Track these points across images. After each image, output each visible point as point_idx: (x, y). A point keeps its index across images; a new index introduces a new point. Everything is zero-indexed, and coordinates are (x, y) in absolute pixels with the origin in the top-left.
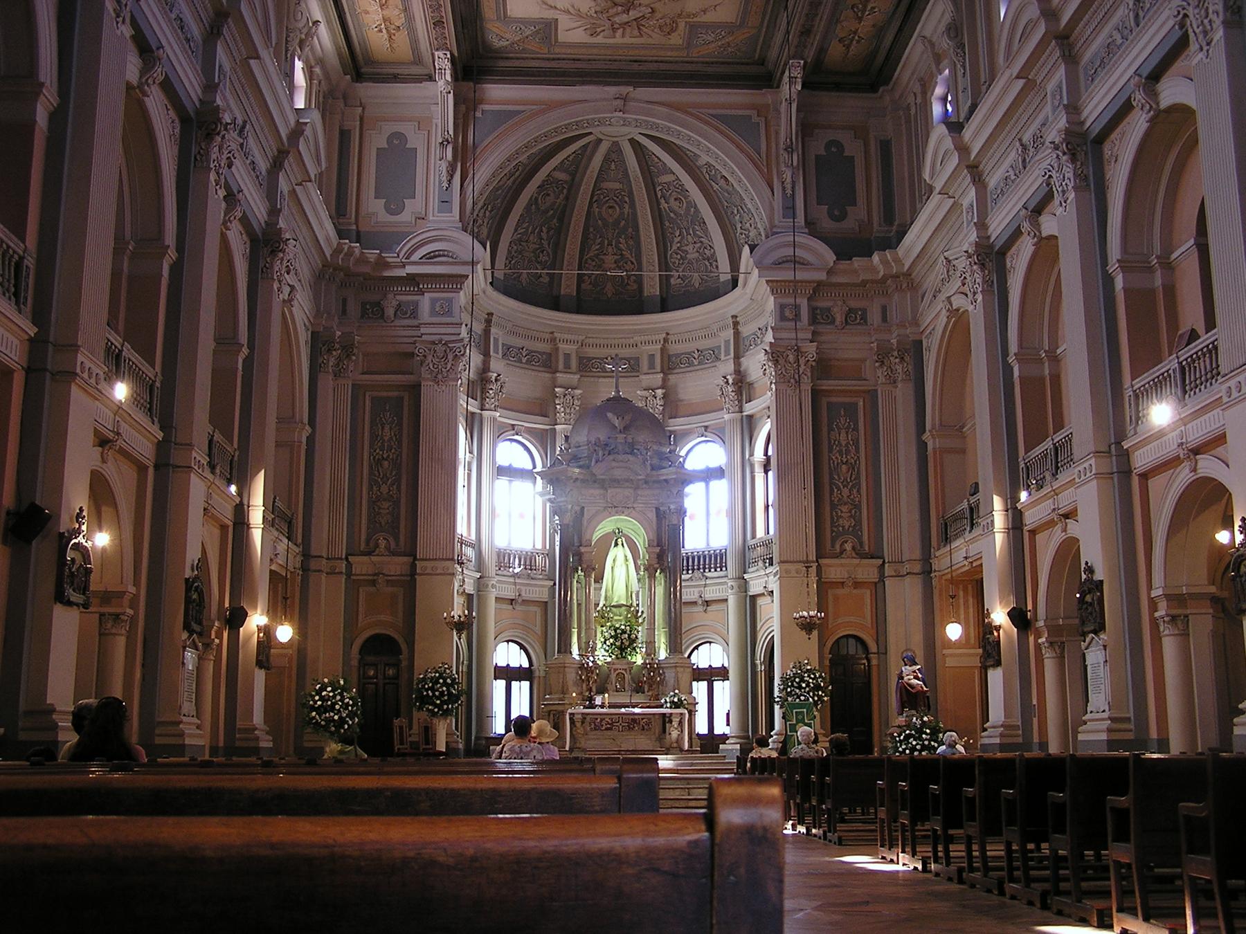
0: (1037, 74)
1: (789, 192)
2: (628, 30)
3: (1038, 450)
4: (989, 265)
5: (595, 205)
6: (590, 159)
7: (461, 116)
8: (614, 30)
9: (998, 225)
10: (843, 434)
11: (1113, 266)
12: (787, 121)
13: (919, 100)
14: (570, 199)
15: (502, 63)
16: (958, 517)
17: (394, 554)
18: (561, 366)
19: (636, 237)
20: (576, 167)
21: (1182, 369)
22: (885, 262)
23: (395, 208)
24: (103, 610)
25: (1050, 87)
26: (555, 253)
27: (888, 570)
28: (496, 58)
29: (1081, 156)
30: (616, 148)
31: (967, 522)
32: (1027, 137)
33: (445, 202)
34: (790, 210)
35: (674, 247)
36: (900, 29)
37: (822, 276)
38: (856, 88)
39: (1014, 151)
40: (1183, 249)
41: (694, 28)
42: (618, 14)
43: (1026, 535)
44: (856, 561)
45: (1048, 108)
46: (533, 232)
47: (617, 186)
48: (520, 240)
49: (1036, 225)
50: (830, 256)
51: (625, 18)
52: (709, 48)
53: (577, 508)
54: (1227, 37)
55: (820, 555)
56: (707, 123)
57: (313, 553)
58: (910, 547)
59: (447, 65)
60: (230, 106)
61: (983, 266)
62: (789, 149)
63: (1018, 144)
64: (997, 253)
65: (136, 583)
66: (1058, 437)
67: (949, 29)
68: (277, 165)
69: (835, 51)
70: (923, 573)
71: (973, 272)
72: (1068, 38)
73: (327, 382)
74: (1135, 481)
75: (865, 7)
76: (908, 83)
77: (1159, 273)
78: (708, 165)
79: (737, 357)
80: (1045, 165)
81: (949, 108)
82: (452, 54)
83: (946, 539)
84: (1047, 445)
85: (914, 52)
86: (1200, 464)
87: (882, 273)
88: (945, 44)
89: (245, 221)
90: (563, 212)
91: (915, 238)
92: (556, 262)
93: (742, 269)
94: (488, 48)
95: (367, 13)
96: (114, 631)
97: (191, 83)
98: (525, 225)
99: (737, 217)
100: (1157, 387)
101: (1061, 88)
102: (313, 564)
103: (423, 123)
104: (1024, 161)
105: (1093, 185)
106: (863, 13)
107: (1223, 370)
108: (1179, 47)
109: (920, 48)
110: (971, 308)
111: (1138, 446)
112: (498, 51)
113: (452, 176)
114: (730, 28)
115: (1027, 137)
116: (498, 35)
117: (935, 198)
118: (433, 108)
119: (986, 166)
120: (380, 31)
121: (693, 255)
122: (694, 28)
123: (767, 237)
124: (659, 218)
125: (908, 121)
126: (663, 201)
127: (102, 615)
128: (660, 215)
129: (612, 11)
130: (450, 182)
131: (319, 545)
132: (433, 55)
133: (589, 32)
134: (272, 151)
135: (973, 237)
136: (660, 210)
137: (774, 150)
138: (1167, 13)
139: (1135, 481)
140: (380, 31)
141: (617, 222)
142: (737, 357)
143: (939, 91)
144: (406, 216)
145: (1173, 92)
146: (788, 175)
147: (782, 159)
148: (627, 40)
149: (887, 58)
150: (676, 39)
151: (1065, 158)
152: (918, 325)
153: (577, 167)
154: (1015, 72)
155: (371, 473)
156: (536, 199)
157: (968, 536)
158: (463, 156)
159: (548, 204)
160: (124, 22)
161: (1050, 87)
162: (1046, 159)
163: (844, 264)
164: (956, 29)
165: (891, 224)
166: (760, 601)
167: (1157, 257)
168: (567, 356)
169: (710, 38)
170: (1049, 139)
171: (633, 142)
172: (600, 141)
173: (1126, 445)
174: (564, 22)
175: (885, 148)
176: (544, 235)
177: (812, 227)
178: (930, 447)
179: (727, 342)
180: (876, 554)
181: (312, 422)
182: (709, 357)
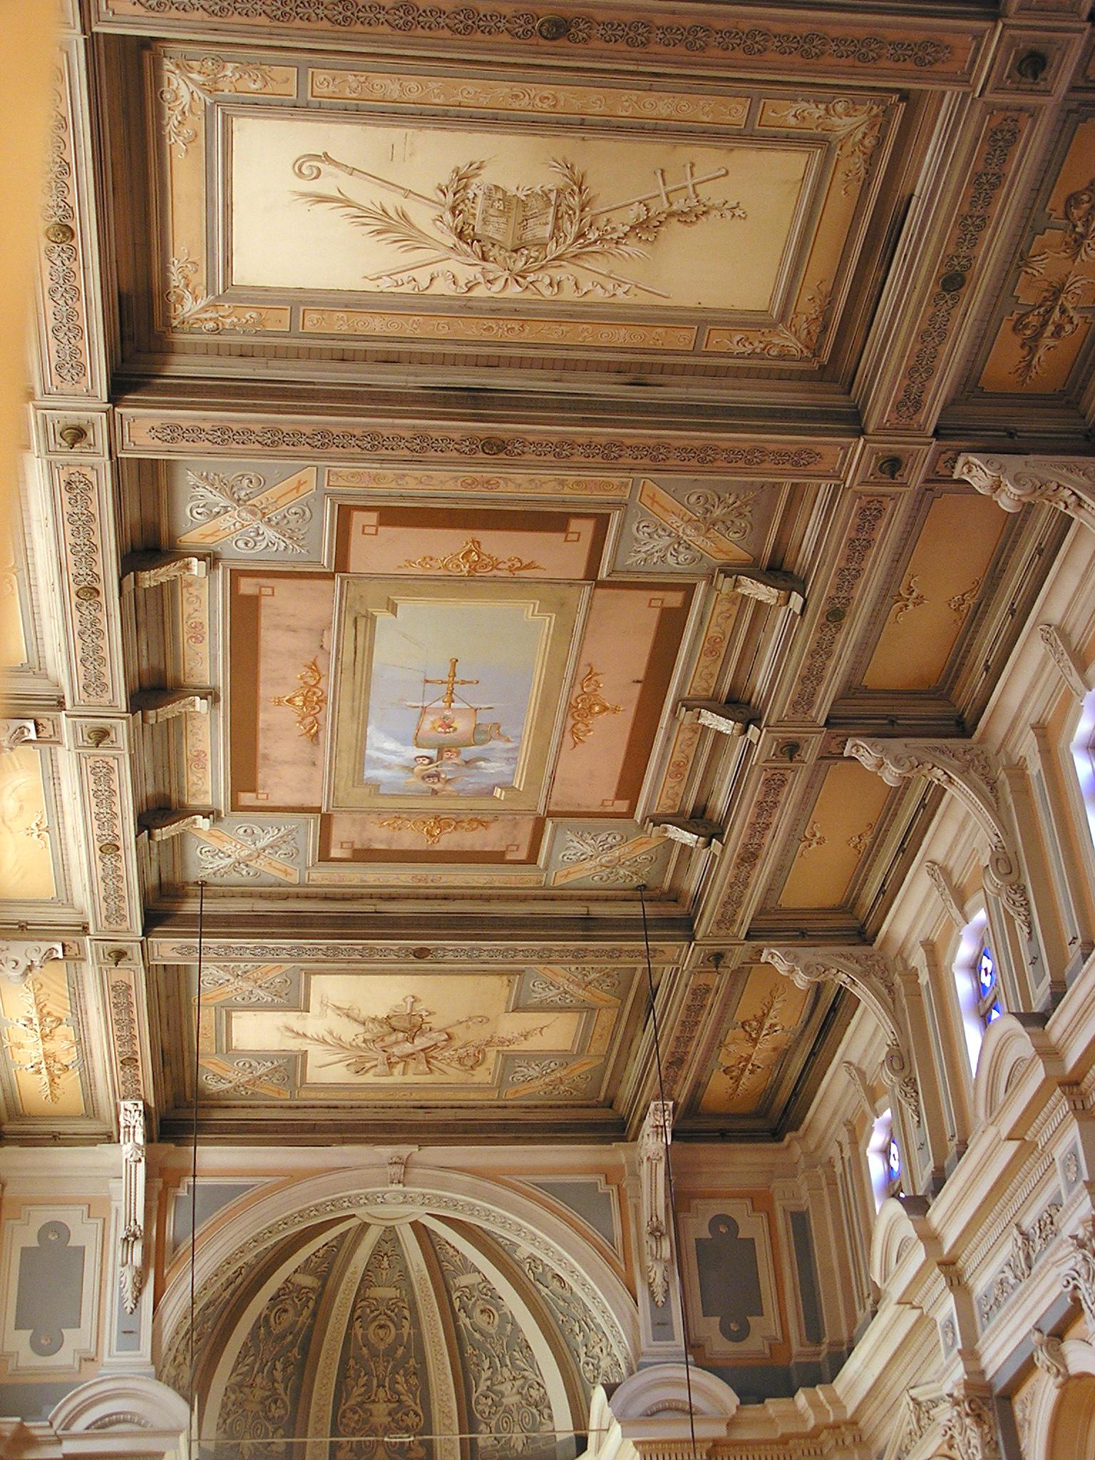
0: (1040, 1134)
1: (660, 1298)
2: (412, 1064)
4: (989, 1416)
5: (358, 1324)
6: (352, 1252)
7: (155, 1196)
8: (391, 1065)
9: (998, 1353)
12: (652, 1195)
13: (847, 1154)
14: (319, 1315)
15: (218, 1114)
19: (421, 1372)
20: (327, 1268)
22: (815, 1404)
23: (46, 1344)
25: (1059, 1152)
26: (295, 1401)
28: (212, 1107)
30: (390, 1236)
32: (1028, 1222)
33: (129, 1333)
34: (661, 1326)
35: (482, 1387)
36: (813, 1053)
37: (720, 1431)
38: (750, 1136)
39: (1011, 1239)
41: (509, 1059)
42: (397, 1043)
45: (1058, 1182)
46: (261, 1370)
47: (390, 1292)
48: (240, 1385)
49: (1058, 1357)
50: (730, 1399)
52: (531, 1086)
56: (529, 1196)
59: (137, 1120)
62: (656, 1233)
63: (1015, 1232)
64: (998, 1397)
67: (890, 1057)
69: (719, 1085)
71: (964, 1429)
72: (1078, 1084)
75: (761, 1024)
76: (828, 1127)
78: (533, 1258)
80: (1065, 1269)
81: (895, 1164)
82: (146, 1105)
85: (836, 1085)
86: (206, 800)
87: (812, 1423)
88: (887, 1078)
90: (308, 1338)
91: (861, 1368)
93: (593, 1424)
94: (198, 1092)
95: (20, 1046)
98: (250, 1360)
99: (580, 1338)
103: (96, 1208)
104: (1028, 1257)
106: (758, 1034)
109: (843, 1077)
112: (210, 1097)
113: (140, 1291)
114: (564, 1058)
115: (1028, 1222)
116: (216, 1075)
117: (888, 1311)
118: (113, 1184)
119: (968, 1263)
120: (39, 1072)
121: (511, 1399)
122: (509, 1059)
123: (631, 1372)
124: (456, 1339)
125: (832, 1182)
126: (462, 1314)
128: (459, 1337)
129: (389, 1040)
130: (137, 1299)
132: (117, 1105)
133: (353, 1068)
135: (959, 1372)
136: (457, 1328)
137: (633, 1230)
140: (39, 1072)
141: (391, 1351)
143: (878, 1139)
144: (65, 1357)
146: (657, 1273)
147: (646, 1249)
148: (410, 1078)
149: (795, 1093)
153: (330, 1269)
154: (1004, 1133)
156: (267, 1318)
158: (158, 1256)
159: (285, 1324)
161: (1059, 1152)
163: (752, 1411)
164: (901, 1059)
165: (819, 1342)
169: (532, 1072)
171: (417, 1227)
172: (365, 1227)
174: (317, 1055)
176: (278, 1375)
177: (696, 1352)
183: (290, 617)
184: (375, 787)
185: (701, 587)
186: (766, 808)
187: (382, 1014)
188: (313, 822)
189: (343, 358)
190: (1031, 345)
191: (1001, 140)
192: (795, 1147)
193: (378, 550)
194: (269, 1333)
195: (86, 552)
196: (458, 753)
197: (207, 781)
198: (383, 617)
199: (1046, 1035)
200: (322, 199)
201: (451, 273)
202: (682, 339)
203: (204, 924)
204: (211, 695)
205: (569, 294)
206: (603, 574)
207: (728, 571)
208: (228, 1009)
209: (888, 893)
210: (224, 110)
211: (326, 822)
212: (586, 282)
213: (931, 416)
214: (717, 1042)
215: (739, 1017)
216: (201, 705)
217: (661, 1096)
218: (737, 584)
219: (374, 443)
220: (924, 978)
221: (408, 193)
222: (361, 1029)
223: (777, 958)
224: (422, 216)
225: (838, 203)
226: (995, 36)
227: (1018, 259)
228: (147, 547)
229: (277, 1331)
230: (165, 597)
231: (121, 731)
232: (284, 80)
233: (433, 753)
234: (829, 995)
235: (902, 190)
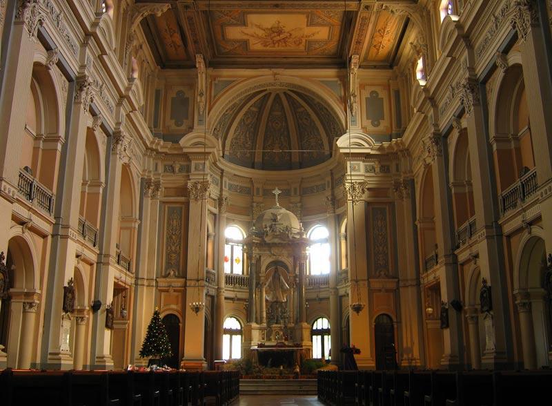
0: (456, 54)
3: (463, 227)
8: (274, 44)
9: (443, 124)
10: (379, 222)
11: (492, 140)
16: (431, 259)
17: (178, 277)
18: (255, 194)
21: (523, 185)
24: (26, 301)
25: (462, 59)
27: (401, 284)
29: (476, 90)
31: (434, 262)
40: (524, 130)
44: (386, 280)
51: (278, 38)
53: (258, 256)
58: (410, 272)
60: (91, 74)
63: (450, 87)
65: (41, 289)
66: (471, 220)
70: (417, 284)
71: (433, 147)
73: (148, 202)
74: (505, 239)
75: (384, 31)
77: (513, 142)
78: (318, 103)
79: (333, 188)
80: (460, 95)
83: (426, 270)
84: (466, 224)
87: (395, 150)
92: (253, 147)
96: (29, 310)
101: (466, 60)
102: (140, 282)
105: (482, 103)
107: (539, 185)
108: (514, 40)
110: (432, 163)
111: (505, 223)
115: (454, 84)
127: (24, 303)
129: (273, 35)
131: (144, 273)
138: (508, 24)
139: (505, 239)
145: (514, 58)
150: (302, 47)
151: (468, 91)
152: (412, 172)
155: (167, 242)
157: (435, 268)
160: (33, 35)
162: (461, 93)
165: (400, 128)
166: (344, 299)
168: (258, 189)
170: (462, 83)
171: (285, 93)
172: (270, 93)
174: (252, 41)
178: (418, 226)
179: (328, 182)
180: (395, 277)
181: (140, 218)
187: (270, 27)
194: (244, 123)
222: (264, 32)
229: (247, 123)
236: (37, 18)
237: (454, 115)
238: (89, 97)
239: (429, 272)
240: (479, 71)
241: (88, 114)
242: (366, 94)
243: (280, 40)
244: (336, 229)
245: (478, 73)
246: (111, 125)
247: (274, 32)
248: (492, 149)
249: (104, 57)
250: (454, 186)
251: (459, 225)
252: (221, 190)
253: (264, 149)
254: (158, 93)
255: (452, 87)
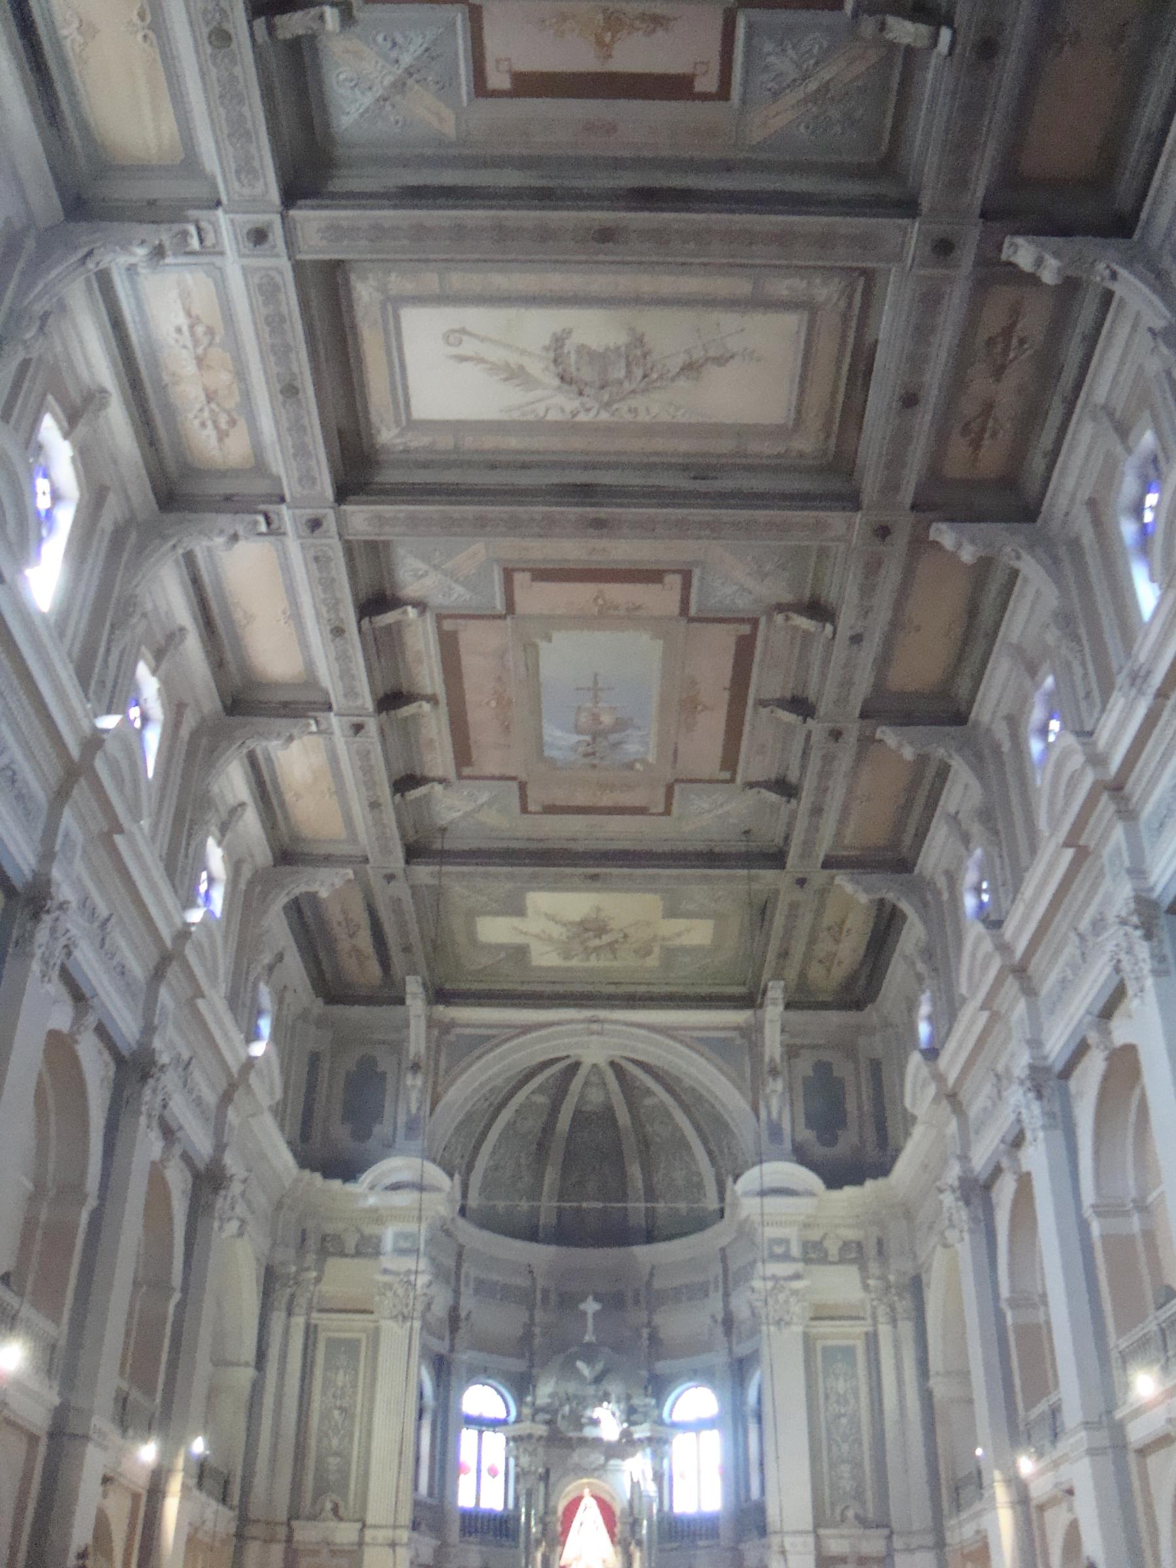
9: (980, 1159)
11: (1088, 1212)
21: (1162, 1331)
27: (898, 1543)
29: (1046, 1092)
32: (1000, 1068)
43: (1033, 1510)
51: (597, 942)
54: (1156, 985)
55: (817, 1525)
57: (252, 1516)
60: (168, 1045)
61: (968, 1203)
68: (226, 1098)
69: (816, 972)
73: (277, 1320)
74: (1132, 1458)
75: (841, 929)
79: (726, 1295)
80: (1110, 947)
82: (424, 978)
83: (958, 1507)
84: (1043, 1407)
86: (439, 772)
89: (186, 1158)
97: (127, 1027)
98: (502, 1151)
100: (1139, 1350)
115: (1084, 925)
119: (964, 1096)
134: (223, 1085)
142: (726, 1295)
150: (652, 962)
167: (1134, 1201)
173: (1119, 1415)
175: (876, 1067)
180: (883, 1523)
182: (700, 1291)
183: (480, 645)
184: (551, 763)
185: (763, 620)
186: (825, 774)
187: (578, 919)
188: (514, 785)
189: (493, 466)
190: (976, 444)
191: (930, 300)
192: (870, 1015)
193: (535, 598)
195: (335, 606)
196: (606, 738)
197: (439, 758)
198: (543, 645)
199: (1002, 935)
200: (462, 359)
201: (557, 404)
202: (726, 445)
203: (445, 856)
204: (433, 699)
205: (643, 417)
206: (693, 611)
207: (780, 608)
208: (471, 915)
209: (921, 835)
210: (394, 302)
211: (523, 787)
212: (654, 407)
213: (907, 496)
214: (812, 941)
215: (825, 925)
216: (426, 707)
217: (777, 976)
218: (787, 618)
219: (514, 526)
220: (945, 896)
221: (523, 352)
222: (564, 930)
223: (843, 881)
224: (536, 368)
225: (827, 346)
226: (915, 228)
227: (957, 383)
228: (376, 601)
230: (393, 635)
231: (372, 725)
232: (430, 281)
233: (588, 738)
234: (888, 909)
235: (869, 339)
236: (63, 941)
237: (1088, 1012)
238: (160, 1097)
239: (964, 1515)
240: (1161, 876)
241: (55, 988)
242: (805, 1066)
243: (600, 947)
244: (733, 1393)
245: (1051, 1051)
246: (127, 1026)
247: (587, 930)
248: (1005, 1322)
249: (118, 838)
250: (1099, 1214)
251: (1029, 1407)
252: (457, 1293)
253: (561, 1198)
254: (314, 1060)
255: (1079, 935)
